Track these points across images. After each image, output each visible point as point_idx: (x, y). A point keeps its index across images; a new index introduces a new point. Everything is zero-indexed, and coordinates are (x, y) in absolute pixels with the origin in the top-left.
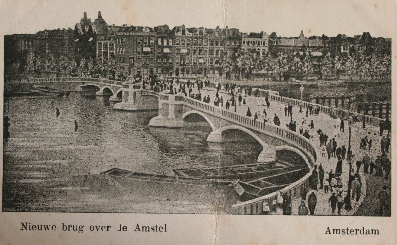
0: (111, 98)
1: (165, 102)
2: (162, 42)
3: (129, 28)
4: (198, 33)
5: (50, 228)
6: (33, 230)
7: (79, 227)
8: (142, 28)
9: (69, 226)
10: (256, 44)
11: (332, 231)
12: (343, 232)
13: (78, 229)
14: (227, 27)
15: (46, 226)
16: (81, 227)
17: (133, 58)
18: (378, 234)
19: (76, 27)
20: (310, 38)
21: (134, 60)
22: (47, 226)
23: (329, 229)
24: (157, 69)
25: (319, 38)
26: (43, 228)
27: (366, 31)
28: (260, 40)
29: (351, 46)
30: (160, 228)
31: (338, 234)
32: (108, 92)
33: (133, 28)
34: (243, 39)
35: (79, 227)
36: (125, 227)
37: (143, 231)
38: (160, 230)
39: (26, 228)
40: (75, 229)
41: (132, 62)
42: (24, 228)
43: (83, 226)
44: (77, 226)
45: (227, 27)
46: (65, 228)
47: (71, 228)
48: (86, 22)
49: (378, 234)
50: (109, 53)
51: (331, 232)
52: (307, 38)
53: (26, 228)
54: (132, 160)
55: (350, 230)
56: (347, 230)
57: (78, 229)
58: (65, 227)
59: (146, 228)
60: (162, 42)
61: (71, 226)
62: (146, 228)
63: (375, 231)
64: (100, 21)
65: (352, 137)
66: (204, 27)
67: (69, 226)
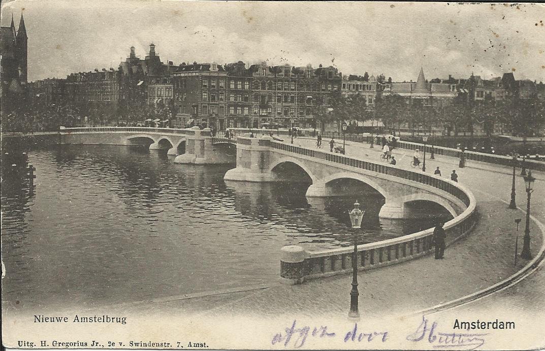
0: (170, 152)
1: (247, 147)
2: (236, 85)
3: (191, 66)
4: (283, 73)
8: (209, 66)
9: (488, 323)
13: (121, 320)
14: (321, 66)
16: (124, 319)
17: (197, 106)
19: (120, 68)
20: (433, 81)
21: (197, 109)
24: (228, 120)
25: (445, 82)
28: (366, 83)
29: (488, 92)
32: (165, 144)
33: (196, 66)
34: (343, 83)
41: (195, 113)
42: (37, 320)
44: (120, 319)
45: (321, 66)
46: (108, 321)
48: (133, 60)
52: (429, 81)
55: (481, 322)
56: (478, 323)
57: (121, 320)
58: (108, 319)
60: (236, 85)
63: (510, 323)
64: (153, 58)
66: (292, 65)
67: (488, 323)
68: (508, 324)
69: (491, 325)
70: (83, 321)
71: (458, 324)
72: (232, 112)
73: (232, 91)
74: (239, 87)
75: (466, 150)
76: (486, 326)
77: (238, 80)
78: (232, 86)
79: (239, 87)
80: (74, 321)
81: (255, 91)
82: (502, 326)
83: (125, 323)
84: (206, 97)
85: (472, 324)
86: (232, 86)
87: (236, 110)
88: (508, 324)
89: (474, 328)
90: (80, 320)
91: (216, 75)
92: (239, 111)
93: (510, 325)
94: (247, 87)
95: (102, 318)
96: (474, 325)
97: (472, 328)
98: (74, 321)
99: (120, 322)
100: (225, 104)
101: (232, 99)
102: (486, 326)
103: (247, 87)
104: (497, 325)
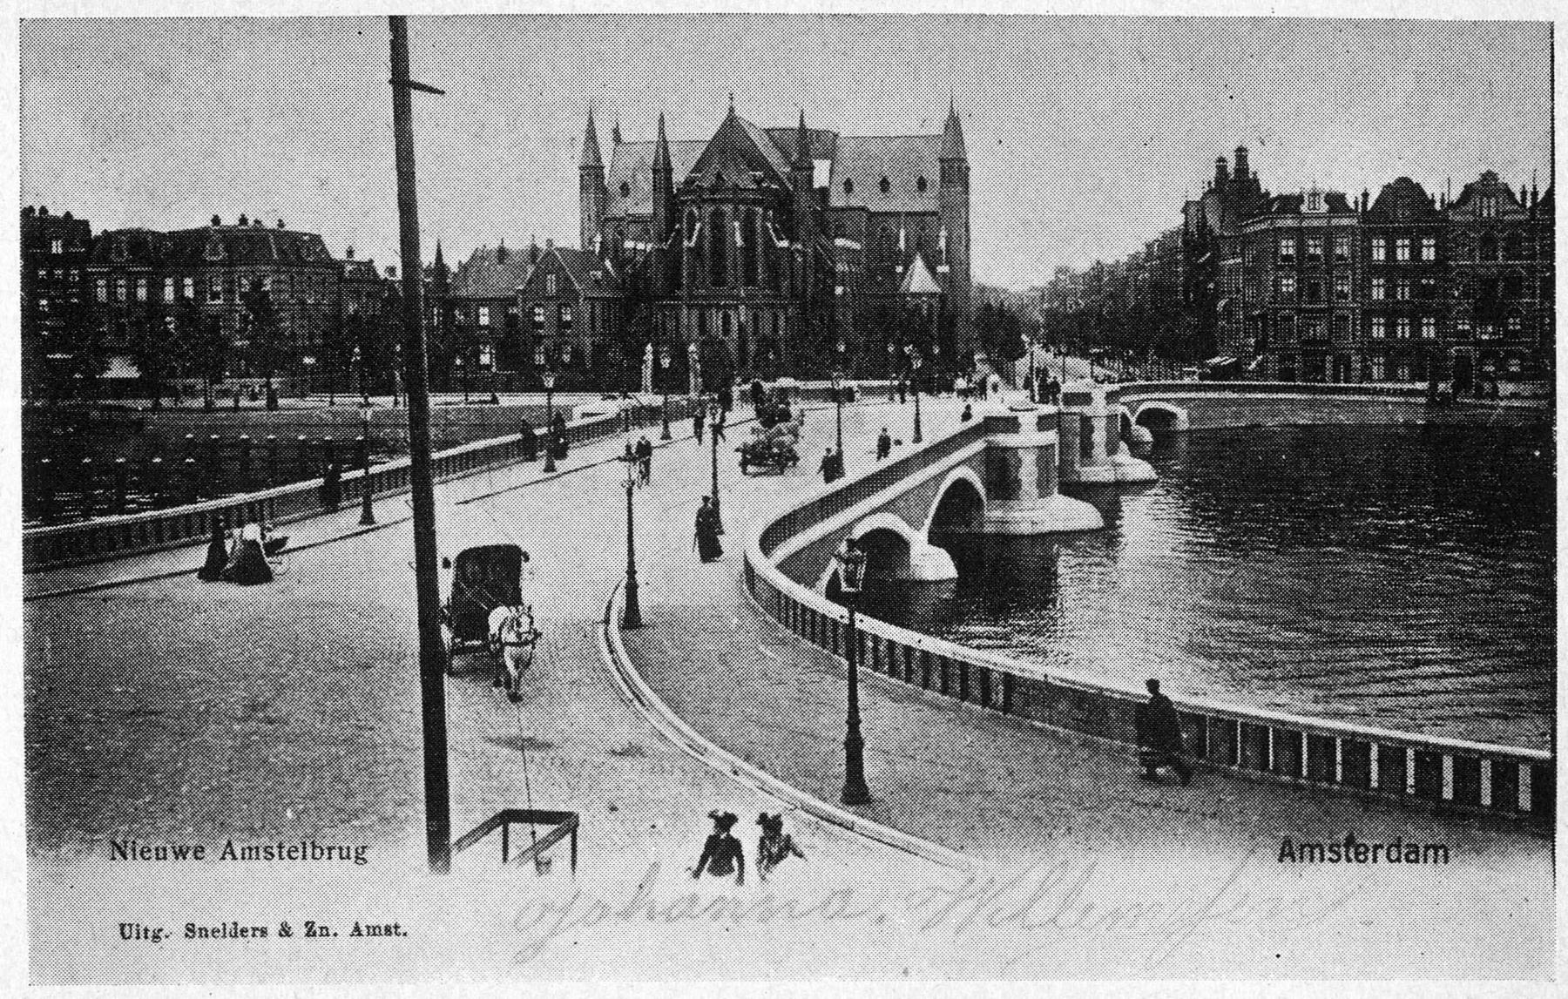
2: (1391, 251)
13: (353, 854)
42: (117, 855)
57: (353, 854)
60: (1391, 251)
68: (1307, 849)
69: (335, 853)
70: (247, 856)
71: (1291, 848)
72: (1379, 332)
73: (1377, 270)
74: (1403, 255)
75: (227, 377)
76: (1370, 855)
77: (1375, 234)
78: (1379, 255)
79: (1403, 255)
80: (223, 858)
81: (1458, 266)
82: (1412, 857)
83: (360, 859)
84: (1291, 289)
85: (273, 855)
86: (1379, 255)
87: (1391, 327)
88: (1307, 849)
89: (1337, 861)
90: (364, 932)
91: (1323, 223)
92: (1403, 331)
93: (1312, 852)
94: (1429, 254)
95: (301, 850)
96: (1335, 852)
97: (1331, 859)
98: (223, 858)
99: (348, 857)
100: (1353, 309)
101: (1378, 294)
102: (1370, 855)
103: (1429, 254)
104: (1400, 853)
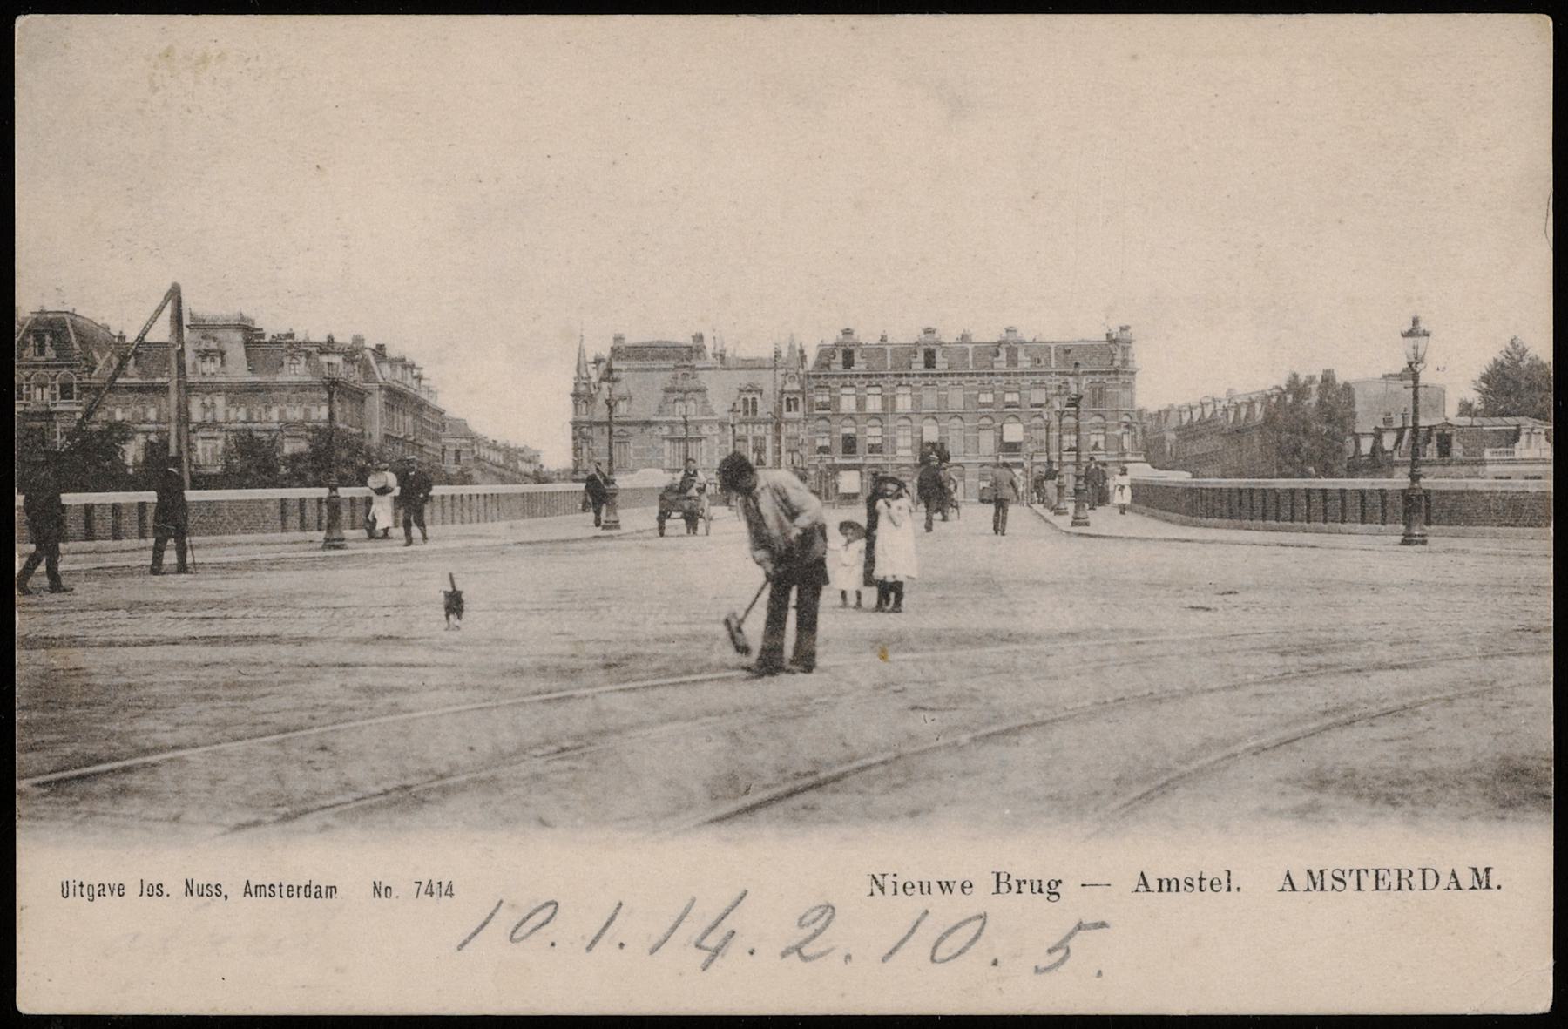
5: (957, 889)
6: (1213, 890)
7: (1049, 884)
10: (1493, 453)
11: (1154, 885)
12: (1190, 885)
13: (1045, 888)
15: (944, 885)
18: (929, 892)
22: (947, 883)
23: (1455, 877)
26: (935, 887)
27: (1328, 368)
30: (963, 885)
31: (1173, 894)
35: (1049, 884)
36: (967, 884)
37: (1161, 890)
38: (1214, 887)
39: (882, 889)
40: (1036, 889)
43: (1060, 881)
47: (1026, 888)
49: (929, 892)
50: (889, 353)
51: (938, 885)
53: (882, 889)
54: (1428, 724)
57: (1045, 888)
59: (1169, 883)
61: (1025, 882)
62: (1169, 883)
65: (1401, 660)
